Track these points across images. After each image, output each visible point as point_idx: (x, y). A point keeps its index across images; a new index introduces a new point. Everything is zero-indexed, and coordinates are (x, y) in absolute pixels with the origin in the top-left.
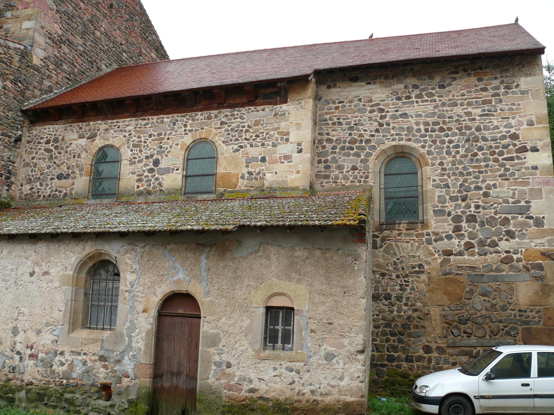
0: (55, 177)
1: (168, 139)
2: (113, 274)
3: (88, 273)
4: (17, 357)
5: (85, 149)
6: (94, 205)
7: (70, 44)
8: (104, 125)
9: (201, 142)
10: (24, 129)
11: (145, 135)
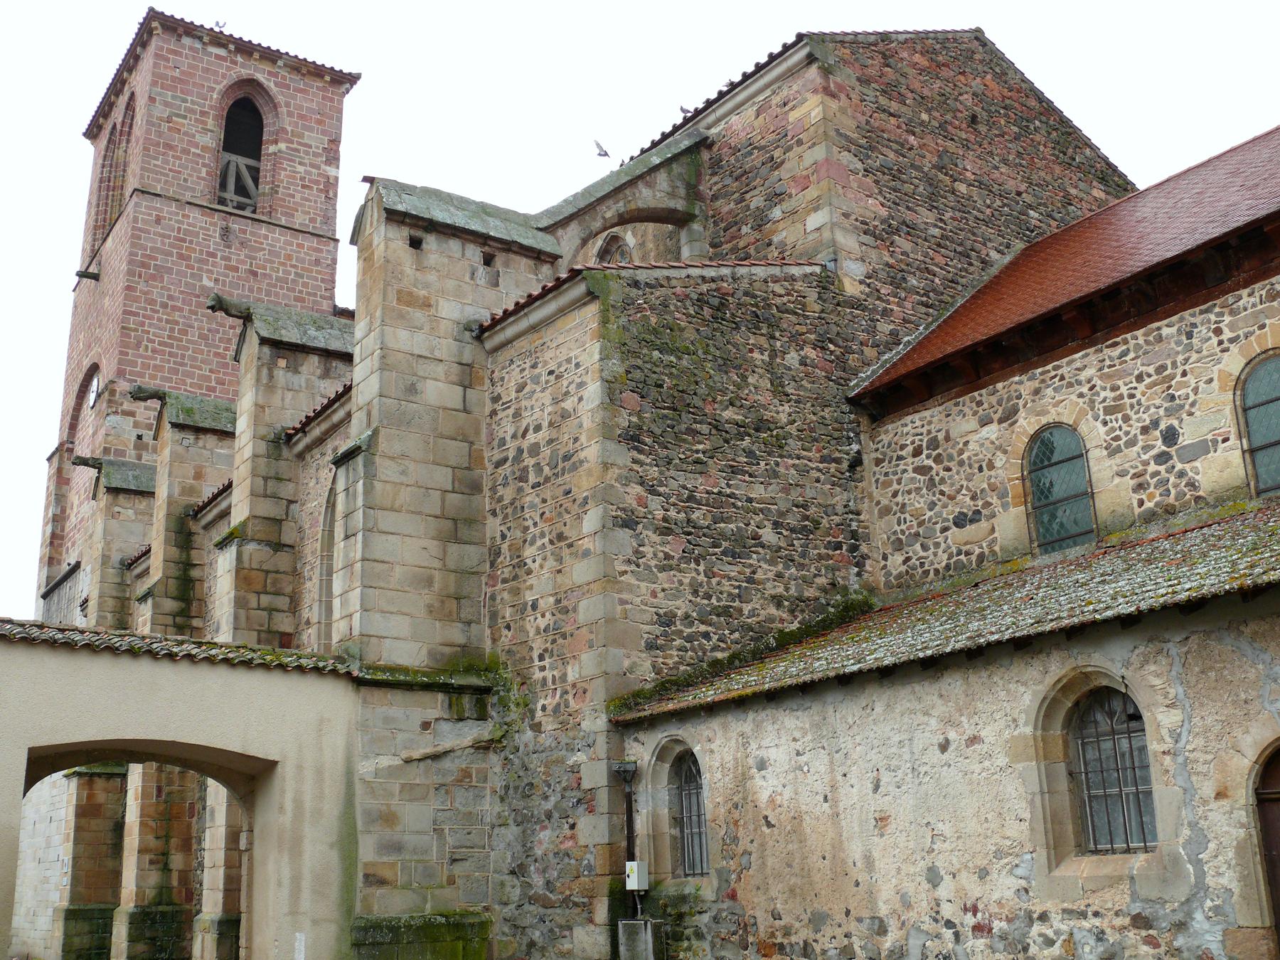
0: (951, 524)
1: (1184, 374)
2: (1124, 718)
3: (1067, 723)
4: (948, 934)
5: (999, 448)
6: (1049, 566)
7: (911, 229)
8: (1029, 383)
9: (1267, 359)
10: (862, 437)
11: (1127, 380)
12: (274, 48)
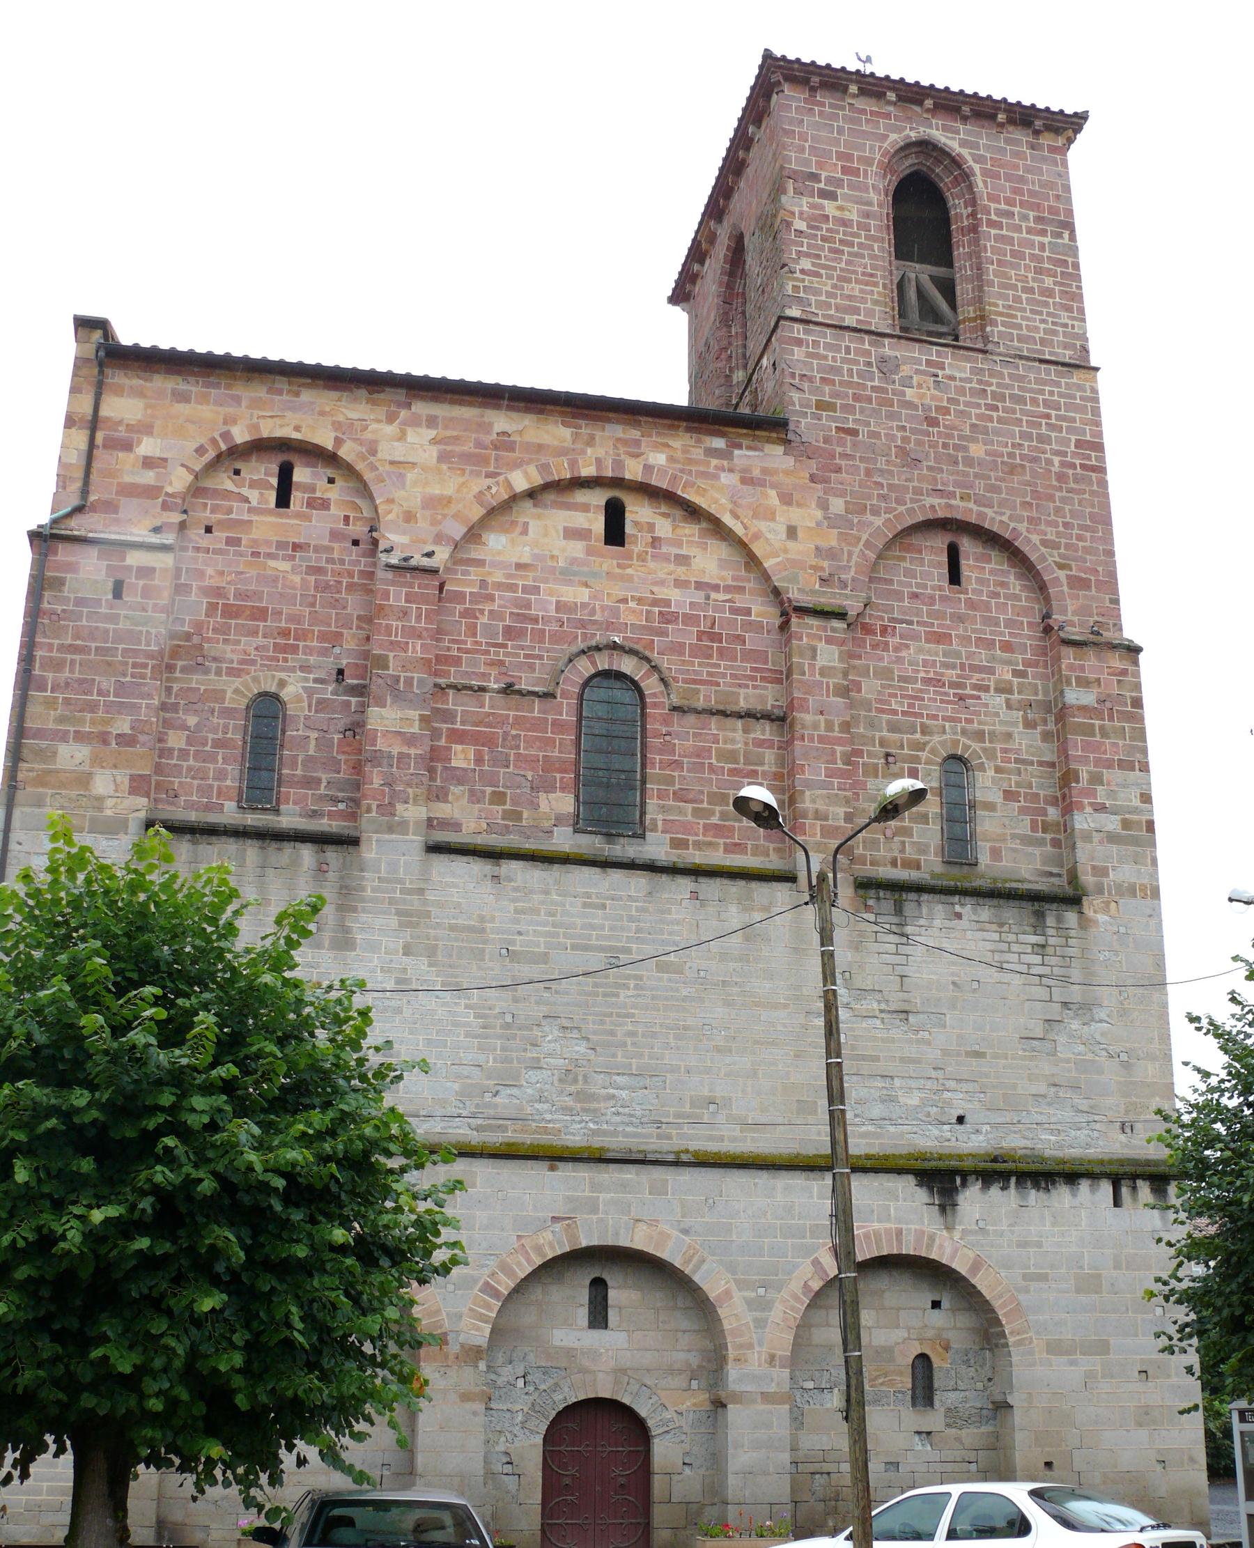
12: (955, 89)
